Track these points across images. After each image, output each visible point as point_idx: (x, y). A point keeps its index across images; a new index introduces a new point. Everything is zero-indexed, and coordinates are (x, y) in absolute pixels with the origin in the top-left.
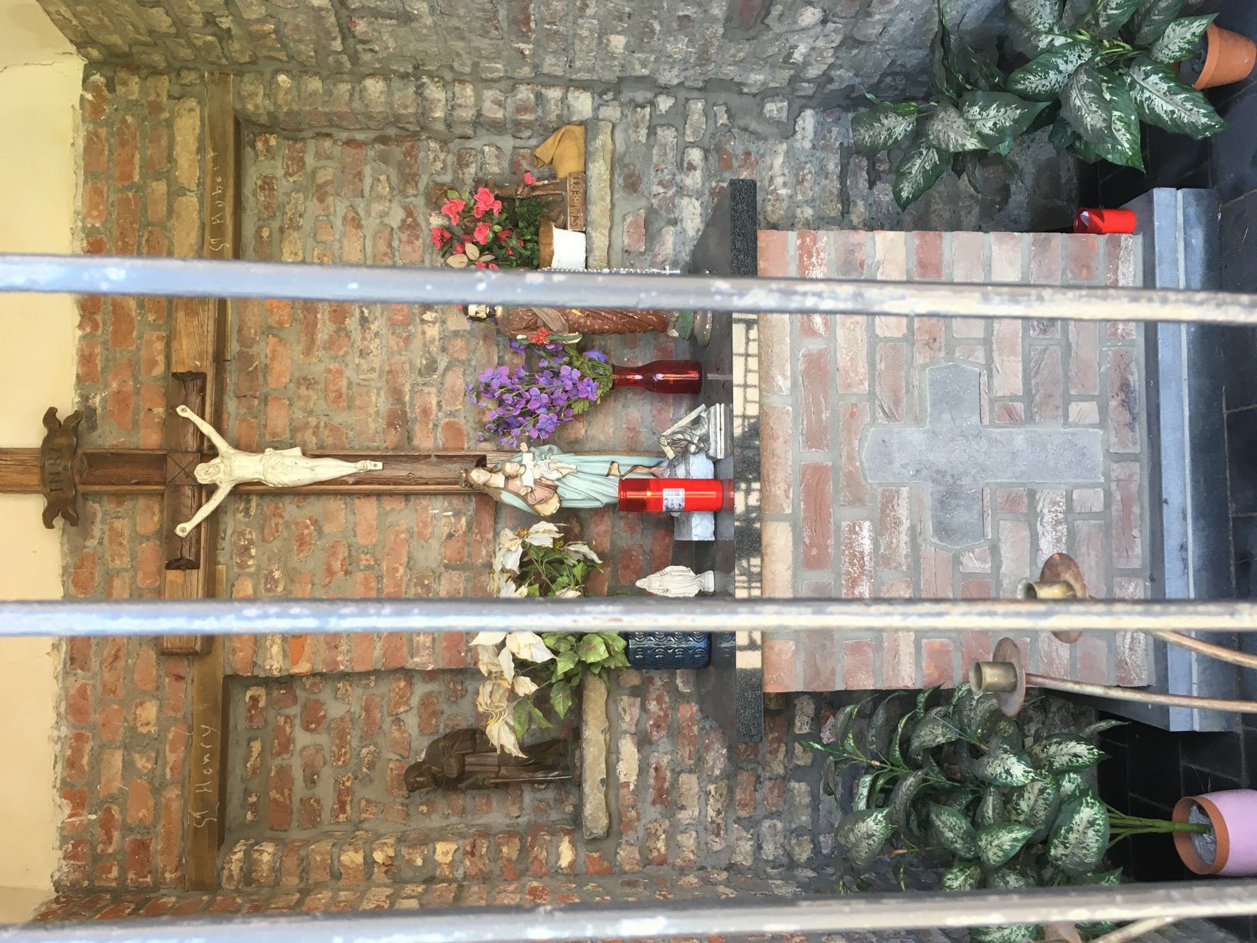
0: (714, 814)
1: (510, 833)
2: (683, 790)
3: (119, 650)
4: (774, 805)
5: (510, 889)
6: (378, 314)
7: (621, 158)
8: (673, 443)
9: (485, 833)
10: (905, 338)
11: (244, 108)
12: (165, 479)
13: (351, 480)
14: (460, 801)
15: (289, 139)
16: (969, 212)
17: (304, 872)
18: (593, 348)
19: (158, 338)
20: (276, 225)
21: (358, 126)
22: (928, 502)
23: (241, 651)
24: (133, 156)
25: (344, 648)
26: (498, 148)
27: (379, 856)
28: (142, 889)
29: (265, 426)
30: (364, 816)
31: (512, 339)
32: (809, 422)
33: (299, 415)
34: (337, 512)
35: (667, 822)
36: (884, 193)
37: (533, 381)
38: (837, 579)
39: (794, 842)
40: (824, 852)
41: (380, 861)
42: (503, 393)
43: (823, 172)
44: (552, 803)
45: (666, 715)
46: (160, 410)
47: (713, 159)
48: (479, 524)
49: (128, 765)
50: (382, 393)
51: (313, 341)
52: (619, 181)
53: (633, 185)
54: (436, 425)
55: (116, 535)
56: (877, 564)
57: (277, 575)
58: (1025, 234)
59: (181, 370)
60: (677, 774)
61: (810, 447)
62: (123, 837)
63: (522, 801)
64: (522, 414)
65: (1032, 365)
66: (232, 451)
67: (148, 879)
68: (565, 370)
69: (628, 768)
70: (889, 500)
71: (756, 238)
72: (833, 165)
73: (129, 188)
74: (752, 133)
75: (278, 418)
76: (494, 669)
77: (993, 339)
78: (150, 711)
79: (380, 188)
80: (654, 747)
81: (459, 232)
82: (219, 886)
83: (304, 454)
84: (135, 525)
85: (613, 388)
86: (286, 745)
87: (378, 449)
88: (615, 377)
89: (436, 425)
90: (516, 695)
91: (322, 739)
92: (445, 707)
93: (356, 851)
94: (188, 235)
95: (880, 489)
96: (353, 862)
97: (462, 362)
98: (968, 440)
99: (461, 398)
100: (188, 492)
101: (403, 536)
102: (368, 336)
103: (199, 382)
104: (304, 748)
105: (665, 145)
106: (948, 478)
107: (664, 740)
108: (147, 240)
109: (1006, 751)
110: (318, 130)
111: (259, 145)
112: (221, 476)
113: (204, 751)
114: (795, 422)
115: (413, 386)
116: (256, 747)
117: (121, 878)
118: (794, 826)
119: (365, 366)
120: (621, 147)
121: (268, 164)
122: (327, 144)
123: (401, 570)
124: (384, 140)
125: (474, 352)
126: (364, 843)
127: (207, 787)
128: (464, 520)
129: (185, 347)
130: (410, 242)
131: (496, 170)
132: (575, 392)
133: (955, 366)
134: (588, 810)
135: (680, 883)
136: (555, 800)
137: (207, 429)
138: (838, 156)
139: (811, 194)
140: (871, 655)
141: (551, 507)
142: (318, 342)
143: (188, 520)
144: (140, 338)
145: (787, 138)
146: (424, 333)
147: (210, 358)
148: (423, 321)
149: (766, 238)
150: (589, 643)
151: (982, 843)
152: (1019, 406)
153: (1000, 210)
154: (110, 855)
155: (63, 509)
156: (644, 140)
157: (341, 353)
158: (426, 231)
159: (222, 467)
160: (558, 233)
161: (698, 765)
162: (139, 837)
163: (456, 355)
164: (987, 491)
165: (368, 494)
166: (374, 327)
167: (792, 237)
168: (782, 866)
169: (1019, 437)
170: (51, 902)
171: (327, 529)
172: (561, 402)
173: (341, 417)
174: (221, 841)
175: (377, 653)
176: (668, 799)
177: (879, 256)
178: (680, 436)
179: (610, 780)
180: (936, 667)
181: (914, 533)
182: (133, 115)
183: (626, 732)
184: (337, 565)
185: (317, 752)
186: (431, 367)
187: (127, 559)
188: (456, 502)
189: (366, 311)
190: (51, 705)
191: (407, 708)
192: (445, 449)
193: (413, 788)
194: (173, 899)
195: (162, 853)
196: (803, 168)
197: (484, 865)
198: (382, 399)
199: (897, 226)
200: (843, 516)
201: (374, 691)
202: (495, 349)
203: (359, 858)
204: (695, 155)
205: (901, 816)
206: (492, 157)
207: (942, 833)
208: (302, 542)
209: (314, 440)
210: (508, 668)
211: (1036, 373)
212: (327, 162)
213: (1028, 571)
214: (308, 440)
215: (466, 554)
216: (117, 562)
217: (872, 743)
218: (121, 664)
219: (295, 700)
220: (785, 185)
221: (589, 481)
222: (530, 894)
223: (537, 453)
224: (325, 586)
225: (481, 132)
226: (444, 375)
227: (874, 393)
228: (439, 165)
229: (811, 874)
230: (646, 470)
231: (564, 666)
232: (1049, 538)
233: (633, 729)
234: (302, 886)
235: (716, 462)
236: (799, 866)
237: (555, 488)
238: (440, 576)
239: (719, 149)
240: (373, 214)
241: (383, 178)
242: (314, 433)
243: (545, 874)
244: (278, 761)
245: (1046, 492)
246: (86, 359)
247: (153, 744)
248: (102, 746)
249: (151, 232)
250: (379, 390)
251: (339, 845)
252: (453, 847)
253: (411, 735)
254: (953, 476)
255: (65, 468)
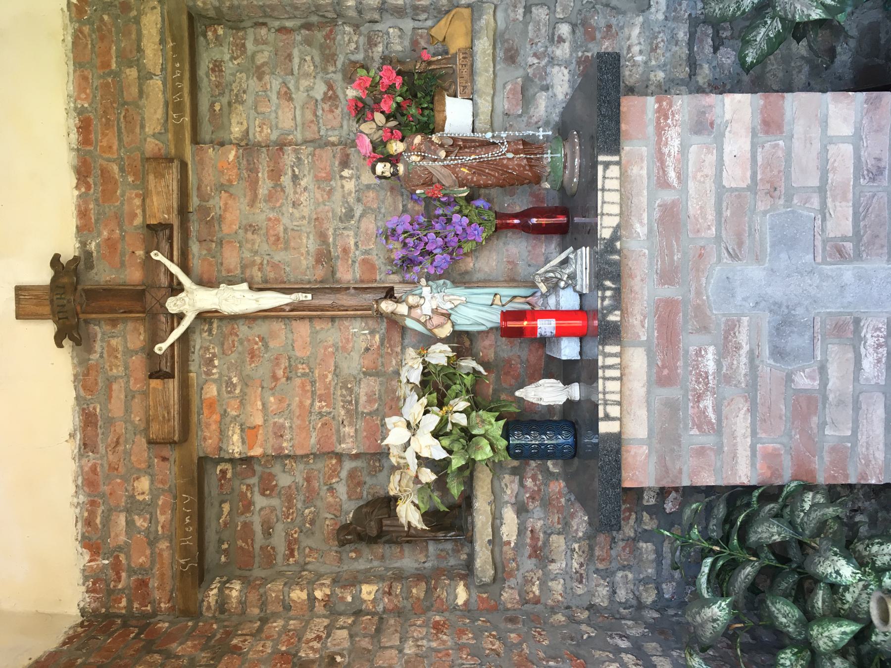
0: (577, 566)
1: (420, 577)
2: (553, 548)
3: (118, 439)
4: (625, 560)
5: (419, 623)
6: (306, 173)
7: (503, 34)
8: (546, 280)
9: (399, 576)
10: (749, 188)
11: (195, 5)
12: (145, 309)
13: (287, 308)
14: (380, 549)
15: (232, 29)
16: (800, 72)
17: (263, 605)
18: (479, 197)
19: (137, 195)
20: (225, 100)
21: (286, 16)
22: (766, 328)
23: (210, 438)
24: (110, 49)
25: (288, 437)
26: (400, 29)
27: (318, 594)
28: (145, 616)
29: (222, 264)
30: (308, 559)
31: (413, 193)
32: (663, 261)
33: (247, 255)
34: (279, 335)
35: (540, 571)
36: (727, 57)
37: (429, 227)
38: (685, 395)
39: (641, 588)
40: (666, 596)
41: (320, 598)
42: (405, 238)
43: (673, 39)
44: (450, 552)
45: (540, 490)
46: (140, 253)
47: (580, 32)
48: (390, 340)
49: (130, 523)
50: (311, 236)
51: (255, 195)
52: (500, 54)
53: (511, 57)
54: (354, 262)
55: (113, 351)
56: (719, 382)
57: (235, 380)
58: (859, 94)
59: (153, 222)
60: (548, 535)
61: (664, 284)
62: (129, 577)
63: (427, 550)
64: (422, 254)
65: (861, 209)
66: (194, 287)
67: (149, 608)
68: (456, 218)
69: (510, 529)
70: (731, 328)
71: (619, 105)
72: (682, 34)
73: (109, 74)
74: (613, 8)
75: (231, 258)
76: (402, 461)
77: (827, 187)
78: (144, 484)
79: (306, 67)
80: (529, 515)
81: (369, 101)
82: (201, 614)
83: (251, 288)
84: (126, 342)
85: (495, 231)
86: (249, 506)
87: (309, 282)
88: (497, 221)
89: (354, 262)
90: (420, 482)
91: (275, 502)
92: (367, 479)
93: (302, 591)
94: (155, 112)
95: (724, 319)
96: (299, 598)
97: (373, 210)
98: (802, 275)
99: (373, 240)
100: (163, 319)
101: (330, 350)
102: (299, 191)
103: (167, 232)
104: (261, 509)
105: (539, 22)
106: (784, 309)
107: (538, 508)
108: (125, 117)
109: (836, 554)
110: (255, 20)
111: (210, 34)
112: (187, 307)
113: (186, 514)
114: (651, 264)
115: (335, 230)
116: (226, 507)
117: (129, 606)
118: (641, 576)
119: (297, 215)
120: (501, 25)
121: (216, 50)
122: (263, 31)
123: (330, 376)
124: (308, 26)
125: (383, 202)
126: (308, 583)
127: (189, 540)
128: (377, 337)
129: (155, 203)
130: (331, 111)
131: (399, 48)
132: (464, 235)
133: (793, 212)
134: (478, 563)
135: (551, 620)
136: (453, 550)
137: (175, 269)
138: (687, 25)
139: (663, 59)
140: (713, 458)
141: (445, 331)
142: (260, 196)
143: (163, 341)
144: (123, 195)
145: (643, 11)
146: (343, 187)
147: (176, 212)
148: (342, 177)
149: (628, 104)
150: (477, 444)
151: (814, 633)
152: (849, 246)
153: (826, 69)
154: (120, 590)
155: (70, 332)
156: (521, 19)
157: (278, 205)
158: (344, 102)
159: (187, 299)
160: (449, 101)
161: (565, 529)
162: (140, 577)
163: (368, 205)
164: (818, 319)
165: (302, 318)
166: (303, 183)
167: (651, 102)
168: (632, 607)
169: (848, 272)
170: (77, 626)
171: (272, 345)
172: (453, 244)
173: (280, 256)
174: (201, 579)
175: (313, 440)
176: (541, 554)
177: (728, 117)
178: (552, 275)
179: (496, 540)
180: (769, 467)
181: (752, 357)
182: (108, 14)
183: (507, 502)
184: (280, 373)
185: (272, 512)
186: (349, 215)
187: (121, 369)
188: (370, 322)
189: (296, 170)
190: (70, 478)
191: (337, 479)
192: (362, 281)
193: (342, 543)
194: (167, 625)
195: (158, 589)
196: (656, 38)
197: (399, 602)
198: (311, 241)
199: (736, 87)
200: (690, 342)
201: (313, 466)
202: (400, 198)
203: (304, 595)
204: (564, 29)
205: (742, 602)
206: (395, 37)
207: (777, 618)
208: (253, 355)
209: (260, 274)
210: (413, 462)
211: (865, 216)
212: (264, 47)
213: (851, 387)
214: (255, 274)
215: (380, 364)
216: (115, 371)
217: (713, 531)
218: (121, 448)
219: (254, 473)
220: (641, 52)
221: (476, 309)
222: (434, 628)
223: (434, 286)
224: (272, 389)
225: (386, 16)
226: (359, 221)
227: (721, 237)
228: (353, 46)
229: (656, 615)
230: (523, 300)
231: (457, 462)
232: (871, 359)
233: (513, 500)
234: (262, 615)
235: (581, 295)
236: (646, 607)
237: (448, 316)
238: (360, 380)
239: (585, 23)
240: (302, 89)
241: (308, 58)
242: (259, 269)
243: (446, 610)
244: (242, 518)
245: (870, 319)
246: (82, 214)
247: (147, 508)
248: (110, 510)
249: (127, 110)
250: (308, 234)
251: (290, 584)
252: (375, 588)
253: (342, 500)
254: (788, 307)
255: (69, 302)
